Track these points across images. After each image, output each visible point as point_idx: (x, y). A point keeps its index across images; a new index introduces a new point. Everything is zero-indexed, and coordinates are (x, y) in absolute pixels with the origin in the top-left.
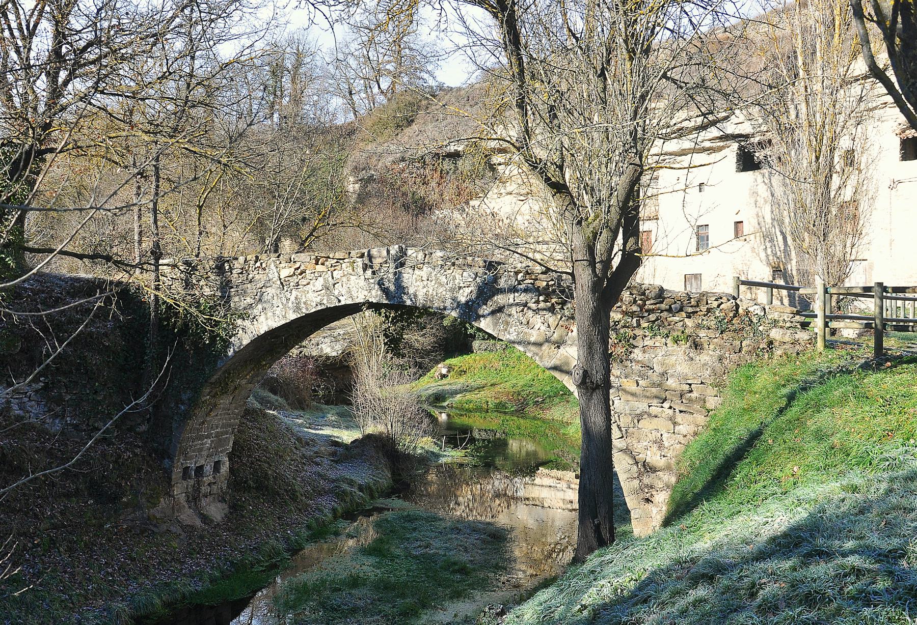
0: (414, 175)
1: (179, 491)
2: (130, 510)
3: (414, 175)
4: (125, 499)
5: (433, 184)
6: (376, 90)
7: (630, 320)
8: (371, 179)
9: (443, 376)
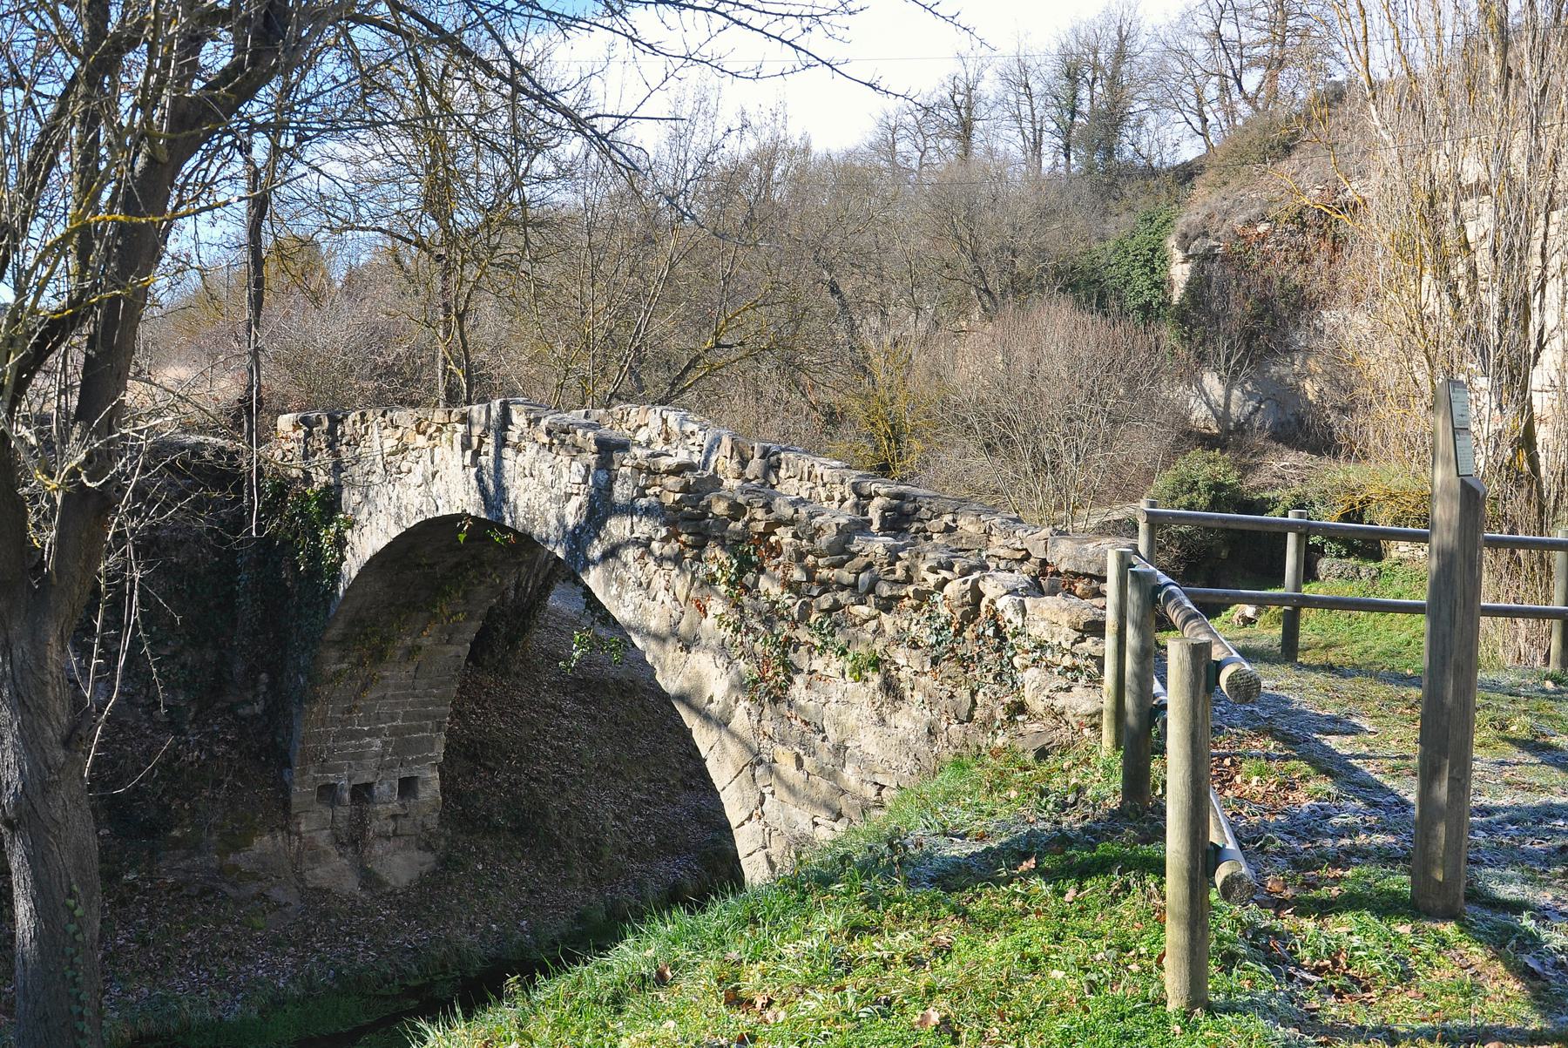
0: (1284, 246)
1: (314, 824)
2: (182, 852)
3: (1284, 246)
4: (176, 833)
5: (1320, 261)
6: (1236, 96)
7: (789, 602)
8: (1208, 256)
9: (1248, 621)
